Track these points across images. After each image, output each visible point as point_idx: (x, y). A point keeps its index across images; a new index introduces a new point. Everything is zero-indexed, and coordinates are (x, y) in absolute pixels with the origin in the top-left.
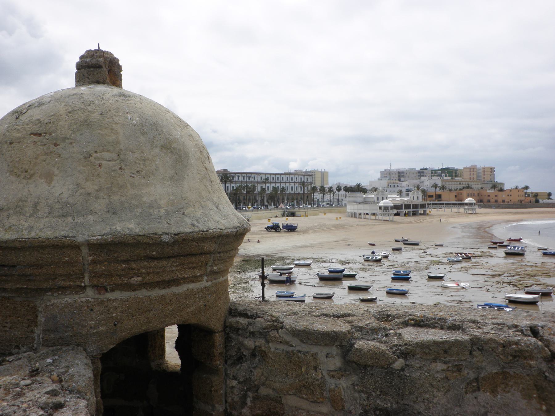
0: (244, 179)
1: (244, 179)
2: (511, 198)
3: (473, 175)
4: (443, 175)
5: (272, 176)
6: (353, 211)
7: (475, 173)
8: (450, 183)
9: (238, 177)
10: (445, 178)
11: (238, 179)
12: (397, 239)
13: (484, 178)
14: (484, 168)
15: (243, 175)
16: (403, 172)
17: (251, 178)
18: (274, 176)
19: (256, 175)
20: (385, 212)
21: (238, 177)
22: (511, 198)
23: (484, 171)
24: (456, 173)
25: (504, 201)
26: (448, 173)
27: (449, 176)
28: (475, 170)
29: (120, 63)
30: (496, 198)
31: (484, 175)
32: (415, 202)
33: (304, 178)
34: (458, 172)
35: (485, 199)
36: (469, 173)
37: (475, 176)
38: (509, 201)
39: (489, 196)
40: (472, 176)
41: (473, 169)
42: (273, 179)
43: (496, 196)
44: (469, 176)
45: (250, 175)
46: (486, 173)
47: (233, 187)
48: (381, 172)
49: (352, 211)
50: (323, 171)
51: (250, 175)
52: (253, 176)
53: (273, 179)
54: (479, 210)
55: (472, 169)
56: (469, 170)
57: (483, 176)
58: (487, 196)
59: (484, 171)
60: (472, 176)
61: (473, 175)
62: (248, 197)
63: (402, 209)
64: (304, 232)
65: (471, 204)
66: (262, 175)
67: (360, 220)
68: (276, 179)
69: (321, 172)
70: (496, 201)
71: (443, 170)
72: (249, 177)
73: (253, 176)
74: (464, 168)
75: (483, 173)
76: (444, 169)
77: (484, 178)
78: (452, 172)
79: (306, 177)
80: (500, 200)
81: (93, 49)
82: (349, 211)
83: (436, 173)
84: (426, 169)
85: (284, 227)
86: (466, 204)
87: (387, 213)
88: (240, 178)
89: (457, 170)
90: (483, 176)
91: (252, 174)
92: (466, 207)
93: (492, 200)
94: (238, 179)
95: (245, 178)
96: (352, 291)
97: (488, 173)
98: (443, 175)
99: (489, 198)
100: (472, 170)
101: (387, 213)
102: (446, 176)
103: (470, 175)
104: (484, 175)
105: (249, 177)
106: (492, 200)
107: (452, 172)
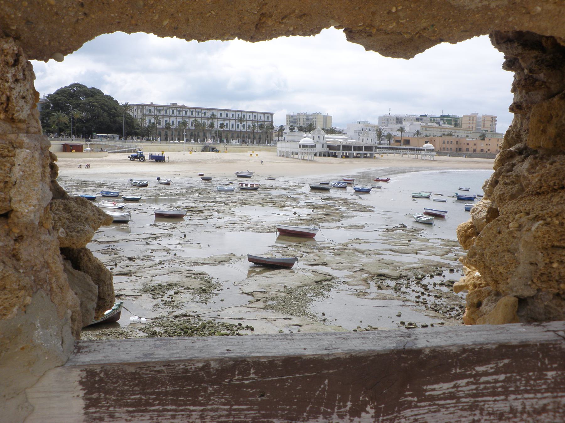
0: (192, 114)
1: (192, 114)
2: (489, 147)
3: (473, 124)
4: (442, 122)
5: (226, 112)
6: (285, 150)
7: (474, 122)
8: (436, 129)
9: (186, 112)
10: (443, 125)
11: (186, 114)
12: (417, 192)
13: (484, 127)
14: (484, 117)
15: (192, 110)
16: (401, 119)
17: (200, 114)
18: (228, 113)
19: (207, 111)
20: (303, 151)
21: (186, 112)
22: (489, 147)
23: (484, 120)
24: (456, 121)
25: (482, 150)
26: (447, 120)
27: (448, 124)
28: (475, 119)
29: (411, 59)
30: (475, 147)
31: (484, 124)
32: (369, 144)
33: (264, 117)
34: (459, 121)
35: (464, 147)
36: (468, 122)
37: (474, 125)
38: (487, 150)
39: (468, 144)
40: (471, 125)
41: (473, 117)
42: (227, 116)
43: (475, 145)
44: (468, 125)
45: (199, 110)
46: (486, 122)
47: (179, 122)
48: (380, 118)
49: (284, 149)
50: (326, 115)
51: (199, 110)
52: (203, 111)
53: (227, 116)
54: (437, 158)
55: (472, 118)
56: (468, 118)
57: (482, 126)
58: (466, 144)
59: (484, 120)
60: (471, 125)
61: (473, 124)
62: (196, 133)
63: (339, 150)
64: (173, 163)
65: (428, 150)
66: (213, 111)
67: (287, 159)
68: (230, 116)
69: (324, 116)
70: (475, 150)
71: (442, 117)
72: (199, 113)
73: (203, 111)
74: (464, 116)
75: (483, 122)
76: (444, 116)
77: (484, 127)
78: (451, 120)
79: (266, 115)
80: (478, 150)
81: (344, 35)
82: (280, 149)
83: (434, 120)
84: (426, 116)
85: (152, 157)
86: (423, 150)
87: (306, 151)
88: (188, 113)
89: (458, 118)
90: (482, 126)
91: (202, 109)
92: (423, 153)
93: (471, 149)
94: (186, 114)
95: (194, 113)
96: (286, 238)
97: (488, 122)
98: (442, 122)
99: (468, 147)
100: (471, 119)
101: (306, 151)
102: (444, 123)
103: (469, 123)
104: (484, 124)
105: (199, 113)
106: (471, 149)
107: (451, 120)
